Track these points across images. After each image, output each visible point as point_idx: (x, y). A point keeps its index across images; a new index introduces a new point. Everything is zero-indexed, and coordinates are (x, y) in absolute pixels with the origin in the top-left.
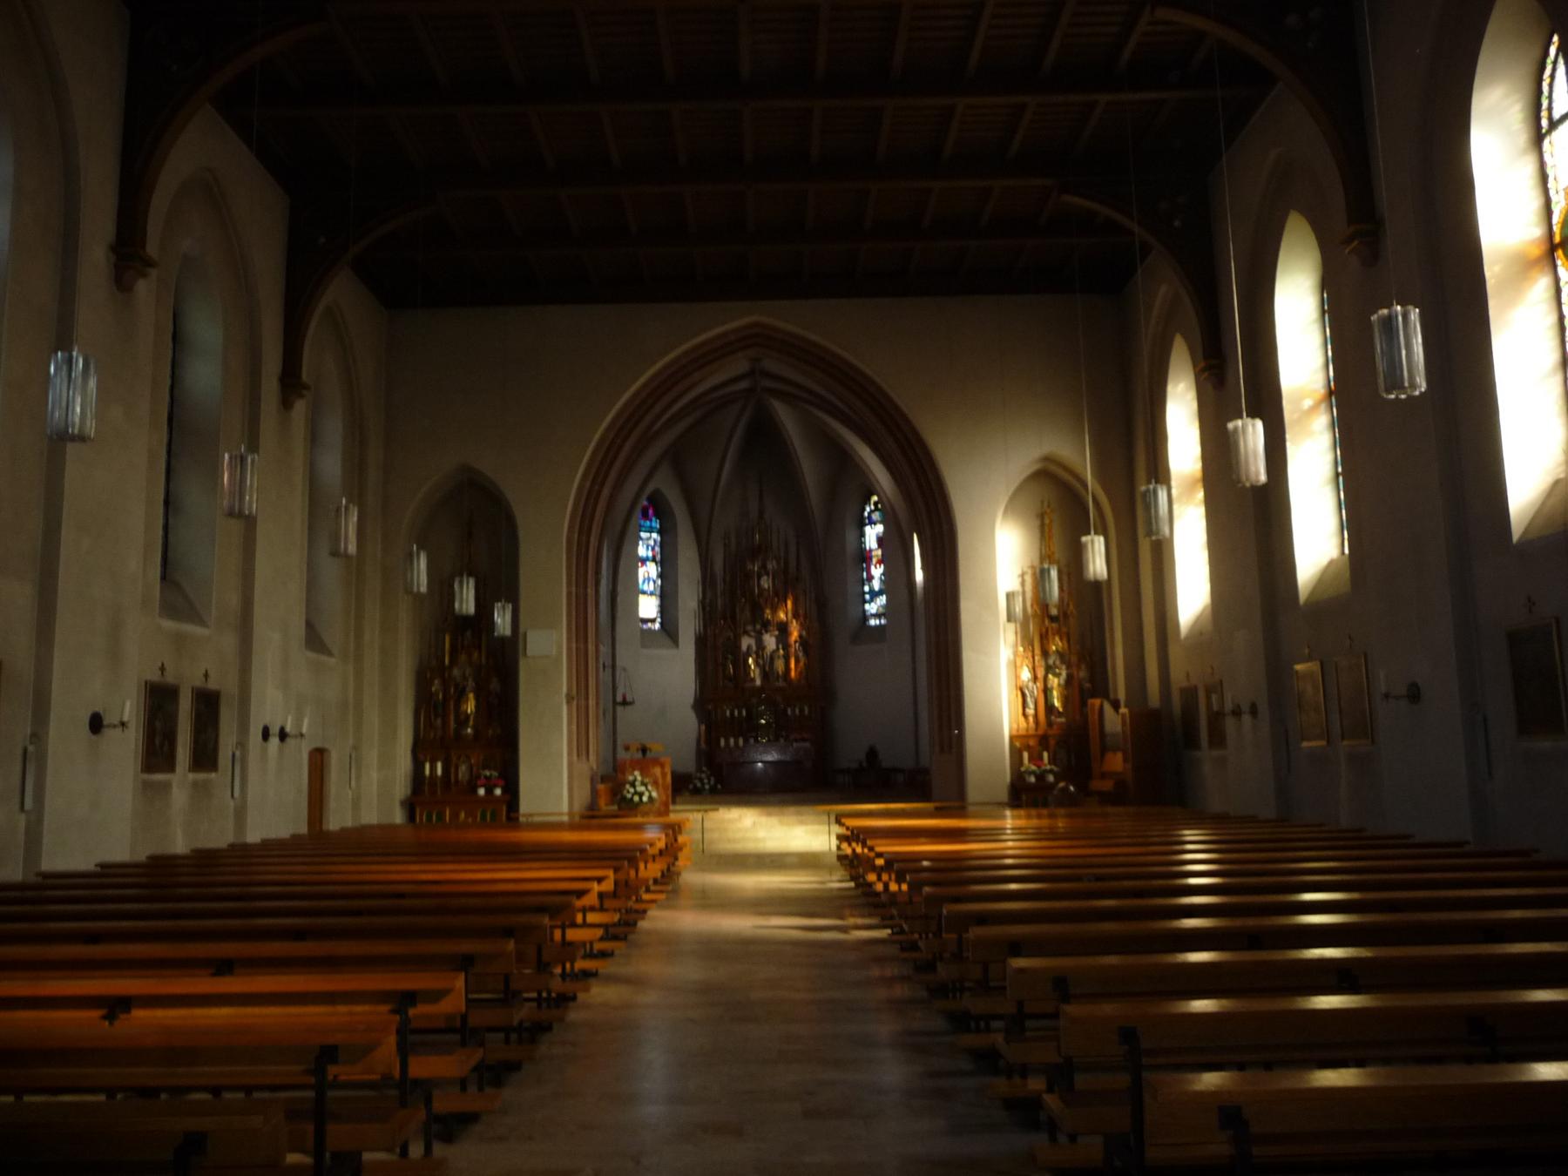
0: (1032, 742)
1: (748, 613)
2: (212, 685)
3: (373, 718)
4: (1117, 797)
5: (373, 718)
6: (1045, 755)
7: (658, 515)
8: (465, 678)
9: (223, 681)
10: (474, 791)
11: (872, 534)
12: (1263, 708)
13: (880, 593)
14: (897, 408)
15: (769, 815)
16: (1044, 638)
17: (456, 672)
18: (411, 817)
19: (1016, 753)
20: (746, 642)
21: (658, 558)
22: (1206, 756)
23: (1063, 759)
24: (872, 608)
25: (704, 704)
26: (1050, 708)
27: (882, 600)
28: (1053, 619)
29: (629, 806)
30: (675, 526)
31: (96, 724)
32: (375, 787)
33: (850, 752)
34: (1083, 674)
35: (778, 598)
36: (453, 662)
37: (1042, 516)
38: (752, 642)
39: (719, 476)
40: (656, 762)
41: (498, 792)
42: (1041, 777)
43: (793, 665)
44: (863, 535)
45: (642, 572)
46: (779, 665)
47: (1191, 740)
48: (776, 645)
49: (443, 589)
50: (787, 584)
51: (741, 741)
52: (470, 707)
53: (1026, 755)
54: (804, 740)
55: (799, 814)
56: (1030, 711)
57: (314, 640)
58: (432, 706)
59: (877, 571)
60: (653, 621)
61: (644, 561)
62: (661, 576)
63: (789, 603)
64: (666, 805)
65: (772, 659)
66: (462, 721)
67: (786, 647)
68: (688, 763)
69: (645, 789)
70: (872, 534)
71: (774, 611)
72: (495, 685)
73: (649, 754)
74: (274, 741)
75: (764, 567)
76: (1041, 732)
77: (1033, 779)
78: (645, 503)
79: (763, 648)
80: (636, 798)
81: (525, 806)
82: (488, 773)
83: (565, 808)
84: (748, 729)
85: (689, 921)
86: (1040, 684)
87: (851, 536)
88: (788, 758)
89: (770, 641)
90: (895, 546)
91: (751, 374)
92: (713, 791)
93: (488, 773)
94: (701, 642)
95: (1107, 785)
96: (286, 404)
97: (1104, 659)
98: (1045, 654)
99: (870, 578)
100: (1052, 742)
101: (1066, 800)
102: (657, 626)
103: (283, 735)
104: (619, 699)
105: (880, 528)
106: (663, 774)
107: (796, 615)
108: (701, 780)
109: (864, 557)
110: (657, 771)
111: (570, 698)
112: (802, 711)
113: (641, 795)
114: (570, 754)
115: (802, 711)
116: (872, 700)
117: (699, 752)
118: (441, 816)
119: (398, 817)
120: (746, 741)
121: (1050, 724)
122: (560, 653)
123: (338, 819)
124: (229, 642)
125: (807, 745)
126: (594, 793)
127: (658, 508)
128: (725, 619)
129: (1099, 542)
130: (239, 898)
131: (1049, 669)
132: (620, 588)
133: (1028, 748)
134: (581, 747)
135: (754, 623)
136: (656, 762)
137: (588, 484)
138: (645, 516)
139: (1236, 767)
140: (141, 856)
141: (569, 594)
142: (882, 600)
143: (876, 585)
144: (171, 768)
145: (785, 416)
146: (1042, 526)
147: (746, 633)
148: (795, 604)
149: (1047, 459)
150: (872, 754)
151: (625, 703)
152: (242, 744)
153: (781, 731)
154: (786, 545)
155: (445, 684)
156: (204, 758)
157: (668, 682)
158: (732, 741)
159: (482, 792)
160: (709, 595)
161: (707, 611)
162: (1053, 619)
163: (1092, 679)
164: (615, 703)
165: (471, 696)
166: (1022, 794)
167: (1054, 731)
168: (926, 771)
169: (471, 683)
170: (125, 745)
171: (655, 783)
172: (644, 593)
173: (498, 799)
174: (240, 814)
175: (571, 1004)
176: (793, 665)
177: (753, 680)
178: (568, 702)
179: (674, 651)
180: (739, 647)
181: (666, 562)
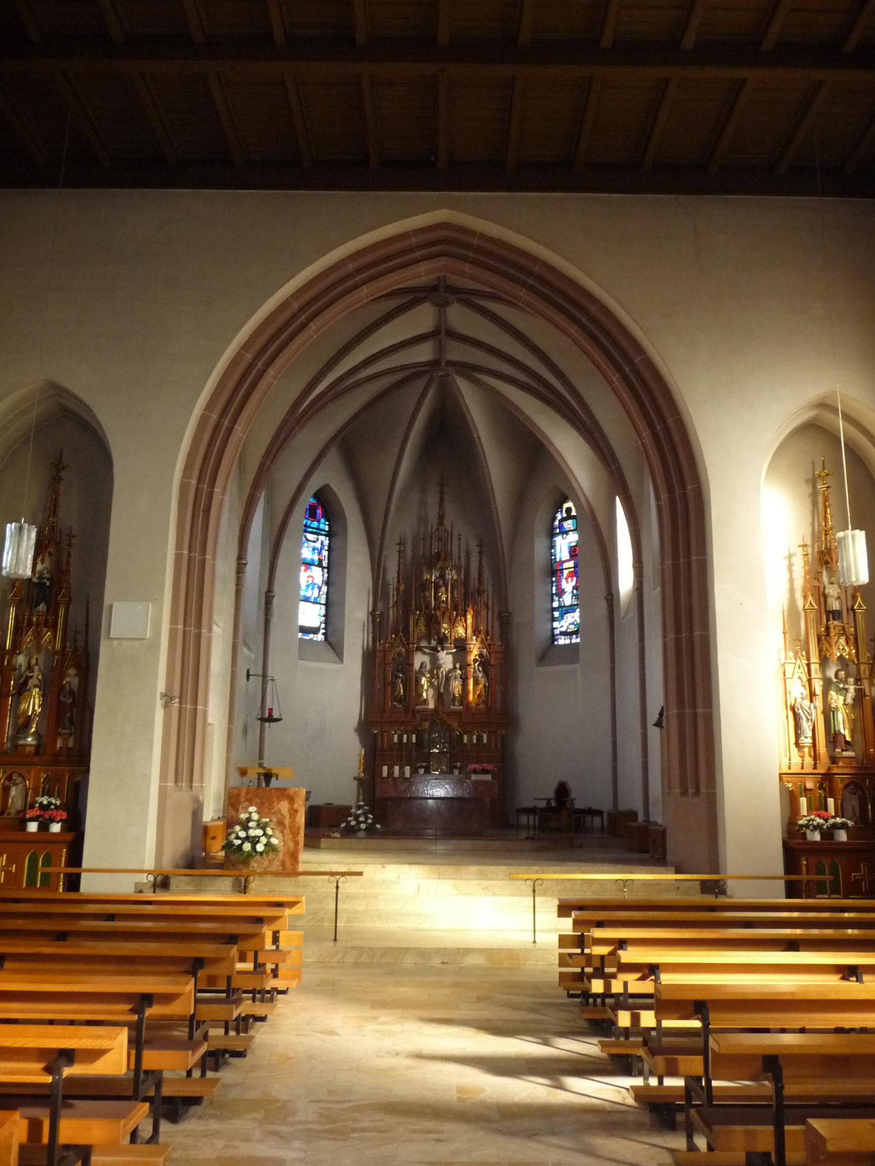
6: (831, 801)
7: (327, 516)
8: (30, 668)
10: (23, 827)
11: (563, 546)
13: (571, 609)
15: (440, 876)
16: (824, 638)
17: (21, 660)
19: (791, 799)
20: (420, 659)
21: (325, 563)
24: (561, 626)
25: (371, 727)
26: (833, 738)
27: (575, 617)
35: (459, 610)
37: (813, 481)
38: (426, 659)
40: (283, 793)
41: (56, 828)
42: (828, 834)
43: (471, 687)
44: (552, 546)
45: (304, 576)
46: (456, 686)
48: (451, 667)
50: (467, 597)
51: (407, 769)
52: (33, 704)
53: (803, 801)
54: (485, 771)
55: (483, 876)
56: (807, 741)
59: (568, 585)
60: (315, 631)
61: (308, 564)
62: (328, 583)
63: (469, 617)
64: (294, 856)
65: (448, 679)
67: (464, 666)
70: (563, 546)
71: (453, 624)
72: (71, 679)
73: (274, 783)
75: (442, 576)
76: (821, 770)
77: (817, 837)
78: (312, 501)
79: (439, 667)
80: (247, 847)
82: (45, 800)
84: (420, 759)
86: (819, 702)
87: (540, 545)
89: (446, 660)
91: (433, 335)
92: (371, 832)
93: (45, 800)
94: (370, 658)
98: (824, 661)
99: (561, 593)
102: (320, 637)
105: (573, 538)
107: (476, 632)
108: (357, 817)
109: (554, 570)
110: (284, 806)
111: (168, 698)
112: (480, 738)
113: (254, 841)
114: (163, 777)
115: (480, 738)
116: (565, 732)
120: (414, 771)
121: (834, 760)
122: (157, 634)
125: (488, 777)
127: (325, 505)
128: (396, 631)
131: (827, 685)
132: (276, 589)
135: (429, 638)
136: (283, 793)
137: (214, 417)
138: (312, 513)
141: (178, 558)
142: (575, 617)
143: (567, 600)
145: (469, 395)
146: (814, 494)
147: (419, 649)
148: (476, 617)
149: (824, 405)
150: (562, 791)
151: (271, 719)
153: (456, 761)
154: (468, 553)
157: (330, 698)
158: (397, 769)
159: (33, 827)
160: (380, 606)
161: (377, 622)
165: (36, 691)
171: (281, 823)
172: (307, 600)
173: (55, 839)
176: (471, 687)
177: (425, 702)
178: (166, 706)
179: (340, 666)
180: (411, 665)
181: (334, 569)
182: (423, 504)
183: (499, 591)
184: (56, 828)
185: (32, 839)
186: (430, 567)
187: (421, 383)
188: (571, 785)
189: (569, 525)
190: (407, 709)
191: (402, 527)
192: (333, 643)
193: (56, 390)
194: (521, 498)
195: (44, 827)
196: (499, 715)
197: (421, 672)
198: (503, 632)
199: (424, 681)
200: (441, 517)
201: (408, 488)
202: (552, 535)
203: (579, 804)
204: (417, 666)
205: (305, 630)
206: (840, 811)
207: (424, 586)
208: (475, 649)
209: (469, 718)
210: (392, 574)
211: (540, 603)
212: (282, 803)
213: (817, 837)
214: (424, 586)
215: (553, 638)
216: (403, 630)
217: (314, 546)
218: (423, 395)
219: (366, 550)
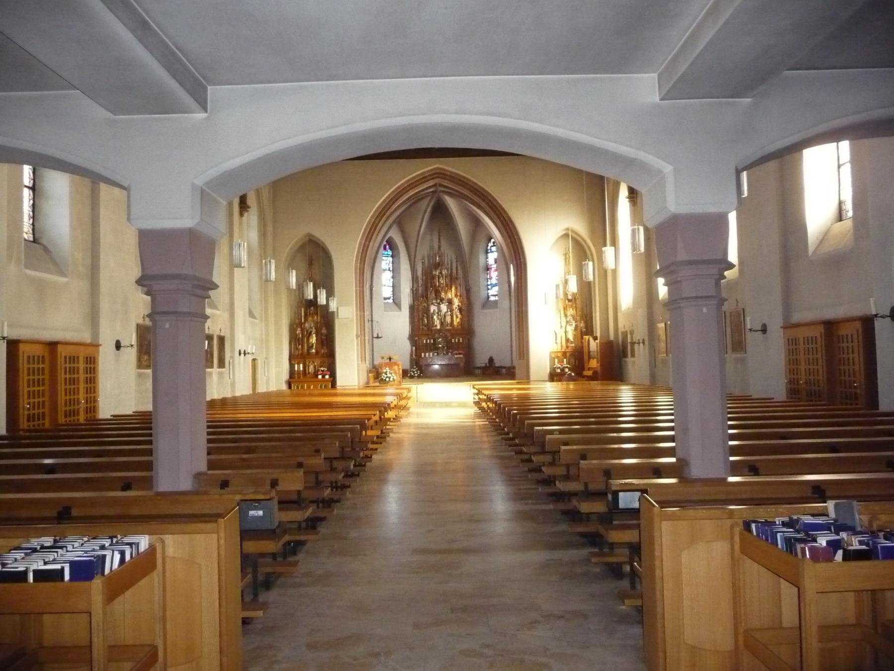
0: (559, 355)
1: (433, 295)
2: (222, 334)
3: (272, 344)
4: (594, 377)
5: (272, 344)
7: (391, 249)
9: (225, 333)
10: (317, 376)
11: (492, 257)
12: (647, 342)
13: (495, 285)
14: (501, 206)
16: (565, 309)
17: (307, 325)
18: (290, 387)
19: (552, 360)
20: (433, 308)
22: (629, 360)
23: (574, 364)
24: (491, 292)
25: (414, 338)
26: (567, 340)
27: (496, 289)
28: (570, 301)
29: (383, 382)
30: (399, 253)
31: (118, 346)
32: (275, 376)
33: (481, 360)
34: (582, 325)
36: (306, 320)
38: (436, 308)
39: (419, 231)
40: (395, 364)
41: (327, 377)
42: (563, 370)
46: (448, 319)
47: (625, 355)
48: (446, 311)
49: (301, 287)
50: (452, 280)
52: (313, 340)
53: (556, 360)
57: (251, 314)
58: (296, 339)
60: (389, 298)
63: (453, 289)
66: (310, 347)
67: (452, 311)
68: (407, 366)
69: (392, 374)
71: (446, 293)
72: (324, 331)
74: (242, 355)
75: (441, 273)
77: (559, 371)
81: (339, 383)
83: (356, 383)
84: (434, 348)
85: (412, 420)
88: (452, 362)
89: (444, 308)
90: (503, 262)
92: (419, 377)
94: (412, 309)
95: (589, 373)
96: (241, 215)
97: (592, 317)
98: (566, 316)
100: (568, 355)
101: (570, 379)
102: (391, 301)
103: (245, 354)
104: (375, 335)
106: (398, 369)
107: (456, 296)
109: (488, 269)
110: (396, 367)
111: (357, 336)
117: (412, 360)
118: (302, 387)
119: (284, 387)
121: (567, 347)
123: (262, 388)
124: (226, 315)
126: (368, 377)
129: (590, 264)
130: (99, 454)
131: (567, 322)
133: (558, 357)
134: (363, 358)
135: (436, 299)
136: (395, 364)
139: (637, 364)
140: (220, 397)
143: (494, 281)
144: (212, 367)
145: (451, 203)
148: (456, 288)
149: (567, 229)
150: (491, 360)
151: (378, 337)
152: (232, 357)
153: (450, 347)
155: (302, 330)
156: (221, 364)
157: (396, 326)
159: (320, 377)
161: (414, 293)
162: (570, 301)
163: (586, 327)
164: (373, 337)
166: (554, 376)
167: (570, 350)
168: (514, 368)
169: (314, 330)
170: (130, 355)
173: (327, 381)
174: (233, 385)
175: (324, 523)
179: (399, 313)
181: (395, 271)
182: (432, 240)
183: (464, 276)
184: (327, 377)
185: (319, 381)
186: (436, 269)
187: (429, 198)
188: (495, 358)
189: (494, 249)
190: (428, 329)
191: (423, 251)
192: (397, 303)
193: (310, 235)
194: (473, 238)
195: (323, 377)
196: (467, 330)
197: (434, 314)
198: (468, 295)
199: (435, 317)
200: (439, 247)
201: (425, 233)
202: (487, 253)
203: (497, 365)
204: (432, 311)
205: (385, 299)
206: (568, 363)
207: (433, 277)
208: (456, 302)
209: (454, 332)
210: (419, 273)
211: (482, 282)
212: (129, 407)
213: (559, 371)
214: (433, 277)
215: (488, 297)
216: (426, 297)
217: (386, 262)
218: (428, 205)
219: (408, 262)
